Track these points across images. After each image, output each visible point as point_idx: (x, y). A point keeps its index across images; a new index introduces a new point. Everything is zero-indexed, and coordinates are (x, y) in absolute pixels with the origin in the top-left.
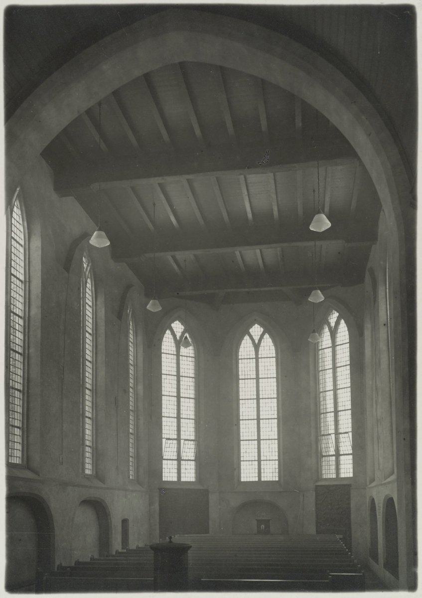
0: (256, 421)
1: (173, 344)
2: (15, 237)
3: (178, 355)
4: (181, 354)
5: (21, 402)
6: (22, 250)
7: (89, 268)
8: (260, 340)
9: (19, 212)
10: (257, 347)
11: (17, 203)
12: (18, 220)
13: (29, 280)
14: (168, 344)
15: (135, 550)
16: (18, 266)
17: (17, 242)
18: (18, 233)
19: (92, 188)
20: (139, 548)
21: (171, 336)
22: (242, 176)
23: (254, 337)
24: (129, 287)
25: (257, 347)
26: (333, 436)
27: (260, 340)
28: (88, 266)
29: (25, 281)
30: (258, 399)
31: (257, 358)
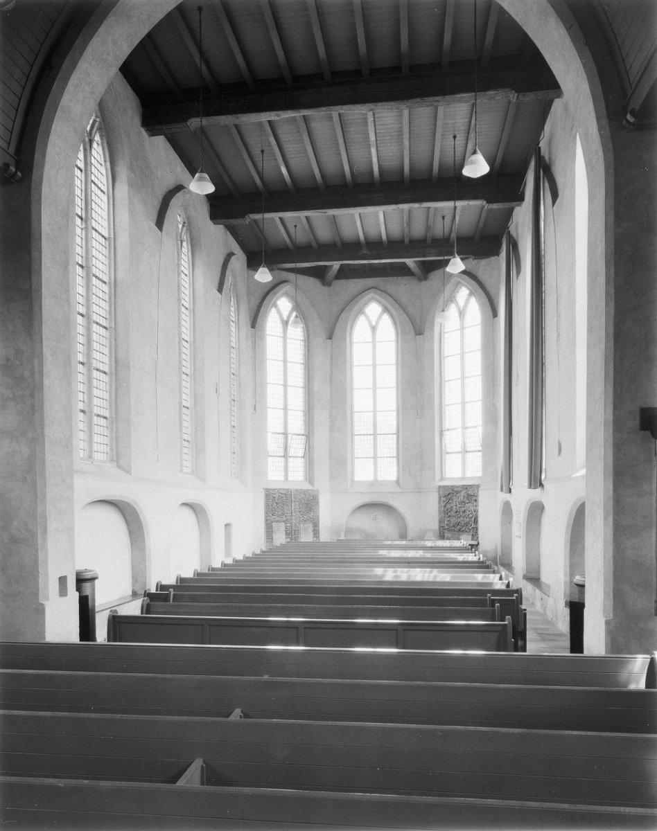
0: (372, 413)
1: (280, 325)
2: (96, 181)
3: (285, 337)
4: (288, 336)
5: (108, 387)
6: (105, 198)
7: (185, 229)
8: (465, 306)
9: (100, 149)
10: (462, 313)
11: (97, 138)
12: (99, 160)
13: (114, 235)
14: (272, 321)
15: (242, 561)
16: (100, 218)
17: (99, 188)
18: (99, 211)
19: (189, 124)
20: (246, 557)
21: (277, 316)
22: (371, 113)
23: (370, 317)
24: (230, 255)
25: (462, 313)
26: (460, 431)
27: (465, 306)
28: (183, 226)
29: (110, 283)
30: (374, 389)
31: (374, 342)
